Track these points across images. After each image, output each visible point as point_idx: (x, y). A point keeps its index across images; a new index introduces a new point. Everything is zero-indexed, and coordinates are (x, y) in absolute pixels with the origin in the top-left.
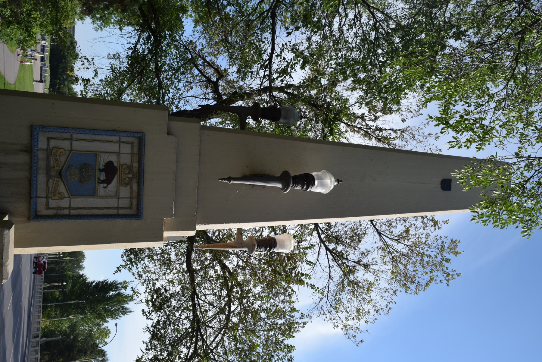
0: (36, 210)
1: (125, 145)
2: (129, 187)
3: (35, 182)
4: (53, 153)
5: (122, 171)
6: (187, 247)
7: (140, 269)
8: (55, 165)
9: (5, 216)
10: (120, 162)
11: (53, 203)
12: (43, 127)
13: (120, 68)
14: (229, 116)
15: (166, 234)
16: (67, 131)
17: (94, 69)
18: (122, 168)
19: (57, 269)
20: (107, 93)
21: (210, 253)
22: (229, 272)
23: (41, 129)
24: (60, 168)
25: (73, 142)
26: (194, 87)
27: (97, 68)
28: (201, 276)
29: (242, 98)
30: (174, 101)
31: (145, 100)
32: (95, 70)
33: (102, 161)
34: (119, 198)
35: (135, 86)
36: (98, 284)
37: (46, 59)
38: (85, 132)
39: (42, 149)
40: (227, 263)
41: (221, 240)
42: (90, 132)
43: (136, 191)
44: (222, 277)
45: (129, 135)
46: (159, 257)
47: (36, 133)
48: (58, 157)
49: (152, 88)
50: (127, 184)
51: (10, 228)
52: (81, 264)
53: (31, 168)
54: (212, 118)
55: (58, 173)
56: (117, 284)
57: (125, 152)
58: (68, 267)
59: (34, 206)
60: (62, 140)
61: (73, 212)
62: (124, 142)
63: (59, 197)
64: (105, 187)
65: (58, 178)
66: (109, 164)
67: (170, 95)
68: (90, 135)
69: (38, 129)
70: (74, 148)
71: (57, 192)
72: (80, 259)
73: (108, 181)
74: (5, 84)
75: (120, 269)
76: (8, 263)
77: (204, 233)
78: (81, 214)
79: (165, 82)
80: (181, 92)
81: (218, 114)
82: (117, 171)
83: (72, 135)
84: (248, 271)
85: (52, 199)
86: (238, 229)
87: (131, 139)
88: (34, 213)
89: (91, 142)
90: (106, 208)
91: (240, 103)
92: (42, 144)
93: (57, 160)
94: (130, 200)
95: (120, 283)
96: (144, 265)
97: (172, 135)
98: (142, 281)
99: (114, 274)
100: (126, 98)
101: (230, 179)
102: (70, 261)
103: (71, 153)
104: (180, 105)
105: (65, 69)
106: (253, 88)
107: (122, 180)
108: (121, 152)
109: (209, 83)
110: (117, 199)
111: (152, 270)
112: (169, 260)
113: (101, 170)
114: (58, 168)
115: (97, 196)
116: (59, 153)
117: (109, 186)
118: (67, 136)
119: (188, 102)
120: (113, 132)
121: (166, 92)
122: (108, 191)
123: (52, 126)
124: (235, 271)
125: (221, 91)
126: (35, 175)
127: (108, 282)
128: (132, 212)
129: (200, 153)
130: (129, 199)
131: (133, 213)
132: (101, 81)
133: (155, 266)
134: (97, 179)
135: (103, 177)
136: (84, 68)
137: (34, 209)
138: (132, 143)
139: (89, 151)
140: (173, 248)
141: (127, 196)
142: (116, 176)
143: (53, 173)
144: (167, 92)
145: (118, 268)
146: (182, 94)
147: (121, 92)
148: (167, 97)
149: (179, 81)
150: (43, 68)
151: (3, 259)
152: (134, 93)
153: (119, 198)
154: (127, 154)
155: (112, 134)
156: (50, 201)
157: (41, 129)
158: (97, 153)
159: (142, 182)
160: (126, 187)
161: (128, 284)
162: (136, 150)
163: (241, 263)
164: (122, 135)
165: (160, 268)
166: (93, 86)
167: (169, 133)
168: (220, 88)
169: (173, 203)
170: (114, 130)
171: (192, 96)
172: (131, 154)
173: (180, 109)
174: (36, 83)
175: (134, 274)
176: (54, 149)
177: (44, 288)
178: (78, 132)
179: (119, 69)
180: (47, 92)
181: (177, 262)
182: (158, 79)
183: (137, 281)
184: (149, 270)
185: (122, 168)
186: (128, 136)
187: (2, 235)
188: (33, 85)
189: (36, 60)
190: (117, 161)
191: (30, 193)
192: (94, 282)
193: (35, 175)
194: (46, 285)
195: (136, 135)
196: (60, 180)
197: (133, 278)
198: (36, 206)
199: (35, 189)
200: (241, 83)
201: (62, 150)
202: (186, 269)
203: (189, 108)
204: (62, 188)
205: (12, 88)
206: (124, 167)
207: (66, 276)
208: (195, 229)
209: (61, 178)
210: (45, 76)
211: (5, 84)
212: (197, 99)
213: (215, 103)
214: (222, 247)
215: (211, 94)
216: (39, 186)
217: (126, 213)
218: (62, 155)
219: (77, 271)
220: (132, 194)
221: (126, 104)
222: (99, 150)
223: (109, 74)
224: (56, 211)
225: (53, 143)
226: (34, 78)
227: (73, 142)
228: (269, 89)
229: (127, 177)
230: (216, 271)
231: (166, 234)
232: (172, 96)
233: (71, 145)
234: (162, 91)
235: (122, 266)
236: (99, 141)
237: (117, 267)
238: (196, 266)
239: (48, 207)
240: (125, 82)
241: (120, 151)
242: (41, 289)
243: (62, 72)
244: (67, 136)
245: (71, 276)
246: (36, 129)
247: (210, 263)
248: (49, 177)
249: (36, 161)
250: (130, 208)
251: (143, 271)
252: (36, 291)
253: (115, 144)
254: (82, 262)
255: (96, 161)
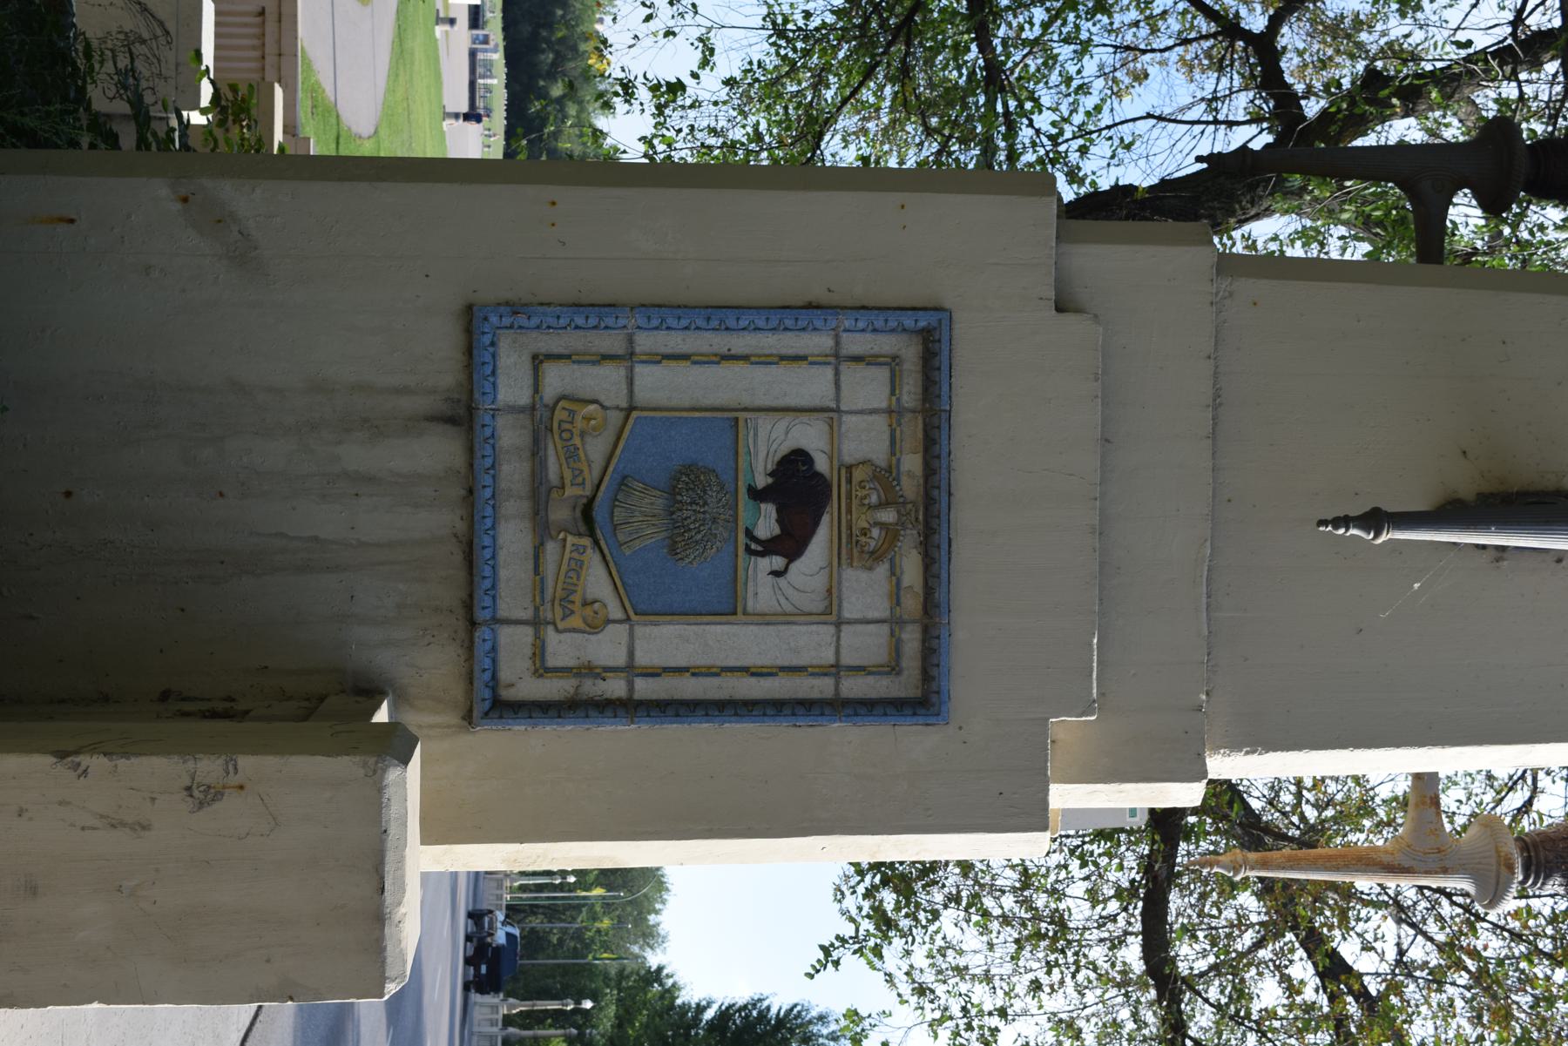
0: (494, 677)
1: (861, 371)
2: (882, 570)
3: (487, 553)
4: (555, 425)
5: (849, 497)
6: (1147, 866)
7: (919, 958)
8: (568, 475)
9: (377, 707)
10: (840, 450)
11: (563, 648)
12: (515, 308)
13: (807, 15)
14: (1351, 201)
15: (1063, 796)
16: (610, 321)
17: (697, 32)
18: (849, 481)
19: (554, 940)
20: (758, 137)
21: (1259, 896)
22: (1362, 995)
23: (506, 321)
24: (588, 492)
25: (638, 369)
26: (1150, 70)
27: (710, 29)
28: (1218, 1007)
29: (1412, 97)
30: (1062, 148)
31: (925, 153)
32: (700, 40)
33: (762, 455)
34: (838, 624)
35: (881, 93)
36: (725, 1015)
37: (489, 15)
38: (684, 323)
39: (513, 409)
40: (1349, 950)
41: (1312, 836)
42: (709, 319)
43: (918, 587)
44: (1326, 1017)
45: (879, 324)
46: (1008, 901)
47: (487, 339)
48: (577, 441)
49: (954, 96)
50: (875, 556)
51: (405, 760)
52: (652, 919)
53: (471, 491)
54: (1257, 217)
55: (578, 513)
56: (810, 1022)
57: (860, 405)
58: (599, 931)
59: (487, 663)
60: (594, 363)
61: (645, 688)
62: (857, 359)
63: (585, 621)
64: (777, 574)
65: (580, 535)
66: (795, 464)
67: (1043, 121)
68: (708, 335)
69: (494, 319)
70: (643, 395)
71: (577, 598)
72: (645, 895)
73: (790, 544)
74: (338, 138)
75: (835, 955)
76: (402, 910)
77: (1226, 796)
78: (677, 696)
79: (1017, 58)
80: (1089, 102)
81: (1289, 194)
82: (829, 496)
83: (630, 340)
84: (1457, 988)
85: (557, 630)
86: (1418, 777)
87: (886, 344)
88: (487, 694)
89: (714, 368)
90: (783, 669)
91: (1404, 130)
92: (512, 387)
93: (572, 454)
94: (892, 634)
95: (822, 1018)
96: (939, 942)
97: (1078, 310)
98: (929, 1016)
99: (811, 976)
100: (839, 150)
101: (1375, 520)
102: (608, 906)
103: (631, 421)
104: (1088, 166)
105: (569, 49)
106: (1469, 43)
107: (850, 536)
108: (843, 408)
109: (1232, 45)
110: (832, 629)
111: (976, 963)
112: (1060, 921)
113: (757, 495)
114: (578, 491)
115: (745, 613)
116: (579, 423)
117: (796, 567)
118: (611, 342)
119: (1128, 147)
120: (811, 310)
121: (1021, 105)
122: (790, 592)
123: (549, 304)
124: (1395, 988)
125: (1289, 79)
126: (489, 522)
127: (768, 1008)
128: (904, 686)
129: (1217, 396)
130: (885, 628)
131: (903, 695)
132: (730, 82)
133: (991, 946)
134: (742, 537)
135: (767, 523)
136: (655, 34)
137: (487, 676)
138: (893, 362)
139: (706, 410)
140: (1075, 864)
141: (876, 615)
142: (825, 519)
143: (560, 513)
144: (1028, 105)
145: (826, 950)
146: (1098, 109)
147: (814, 127)
148: (1025, 134)
149: (1085, 48)
150: (480, 56)
151: (383, 892)
152: (871, 125)
153: (838, 624)
154: (873, 412)
155: (801, 324)
156: (550, 634)
157: (506, 321)
158: (742, 415)
159: (945, 546)
160: (870, 569)
161: (866, 1023)
162: (910, 393)
163: (1419, 951)
164: (847, 324)
165: (1015, 958)
166: (692, 113)
167: (1060, 309)
168: (1289, 64)
169: (1091, 645)
170: (810, 306)
171: (1149, 116)
172: (889, 411)
173: (1093, 183)
174: (453, 121)
175: (890, 978)
176: (562, 404)
177: (508, 1021)
178: (655, 323)
179: (801, 23)
180: (497, 153)
181: (1095, 934)
182: (985, 47)
183: (905, 1015)
184: (962, 962)
185: (849, 481)
186: (875, 330)
187: (380, 789)
188: (443, 133)
189: (452, 22)
190: (827, 448)
191: (469, 606)
192: (734, 1005)
193: (489, 522)
194: (514, 1006)
195: (909, 322)
196: (586, 541)
197: (888, 999)
198: (494, 661)
199: (487, 584)
200: (1397, 27)
201: (592, 407)
202: (1138, 967)
203: (1139, 174)
204: (596, 581)
205: (367, 149)
206: (858, 475)
207: (589, 970)
208: (1198, 773)
209: (591, 533)
210: (488, 89)
211: (338, 138)
212: (1171, 126)
213: (1268, 138)
214: (1327, 869)
215: (1242, 100)
216: (503, 574)
217: (873, 695)
218: (594, 429)
219: (635, 949)
220: (898, 603)
221: (841, 178)
222: (747, 401)
223: (760, 49)
224: (574, 682)
225: (556, 379)
226: (445, 102)
227: (638, 369)
228: (1561, 42)
229: (876, 524)
230: (1292, 988)
231: (1063, 796)
232: (1053, 124)
233: (630, 382)
234: (1005, 105)
235: (842, 940)
236: (745, 358)
237: (822, 947)
238: (1190, 956)
239: (542, 669)
240: (832, 79)
241: (838, 399)
242: (493, 1023)
243: (554, 64)
244: (611, 342)
245: (613, 972)
246: (486, 319)
247: (1259, 944)
248: (542, 529)
249: (488, 462)
250: (893, 668)
251: (933, 965)
252: (476, 1029)
253: (815, 370)
254: (657, 912)
255: (737, 453)
